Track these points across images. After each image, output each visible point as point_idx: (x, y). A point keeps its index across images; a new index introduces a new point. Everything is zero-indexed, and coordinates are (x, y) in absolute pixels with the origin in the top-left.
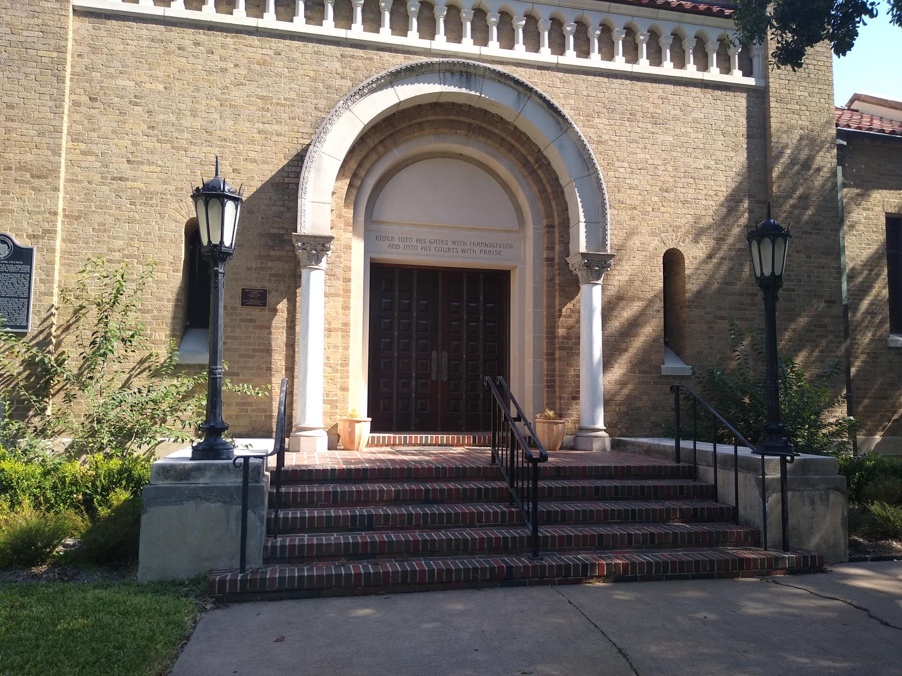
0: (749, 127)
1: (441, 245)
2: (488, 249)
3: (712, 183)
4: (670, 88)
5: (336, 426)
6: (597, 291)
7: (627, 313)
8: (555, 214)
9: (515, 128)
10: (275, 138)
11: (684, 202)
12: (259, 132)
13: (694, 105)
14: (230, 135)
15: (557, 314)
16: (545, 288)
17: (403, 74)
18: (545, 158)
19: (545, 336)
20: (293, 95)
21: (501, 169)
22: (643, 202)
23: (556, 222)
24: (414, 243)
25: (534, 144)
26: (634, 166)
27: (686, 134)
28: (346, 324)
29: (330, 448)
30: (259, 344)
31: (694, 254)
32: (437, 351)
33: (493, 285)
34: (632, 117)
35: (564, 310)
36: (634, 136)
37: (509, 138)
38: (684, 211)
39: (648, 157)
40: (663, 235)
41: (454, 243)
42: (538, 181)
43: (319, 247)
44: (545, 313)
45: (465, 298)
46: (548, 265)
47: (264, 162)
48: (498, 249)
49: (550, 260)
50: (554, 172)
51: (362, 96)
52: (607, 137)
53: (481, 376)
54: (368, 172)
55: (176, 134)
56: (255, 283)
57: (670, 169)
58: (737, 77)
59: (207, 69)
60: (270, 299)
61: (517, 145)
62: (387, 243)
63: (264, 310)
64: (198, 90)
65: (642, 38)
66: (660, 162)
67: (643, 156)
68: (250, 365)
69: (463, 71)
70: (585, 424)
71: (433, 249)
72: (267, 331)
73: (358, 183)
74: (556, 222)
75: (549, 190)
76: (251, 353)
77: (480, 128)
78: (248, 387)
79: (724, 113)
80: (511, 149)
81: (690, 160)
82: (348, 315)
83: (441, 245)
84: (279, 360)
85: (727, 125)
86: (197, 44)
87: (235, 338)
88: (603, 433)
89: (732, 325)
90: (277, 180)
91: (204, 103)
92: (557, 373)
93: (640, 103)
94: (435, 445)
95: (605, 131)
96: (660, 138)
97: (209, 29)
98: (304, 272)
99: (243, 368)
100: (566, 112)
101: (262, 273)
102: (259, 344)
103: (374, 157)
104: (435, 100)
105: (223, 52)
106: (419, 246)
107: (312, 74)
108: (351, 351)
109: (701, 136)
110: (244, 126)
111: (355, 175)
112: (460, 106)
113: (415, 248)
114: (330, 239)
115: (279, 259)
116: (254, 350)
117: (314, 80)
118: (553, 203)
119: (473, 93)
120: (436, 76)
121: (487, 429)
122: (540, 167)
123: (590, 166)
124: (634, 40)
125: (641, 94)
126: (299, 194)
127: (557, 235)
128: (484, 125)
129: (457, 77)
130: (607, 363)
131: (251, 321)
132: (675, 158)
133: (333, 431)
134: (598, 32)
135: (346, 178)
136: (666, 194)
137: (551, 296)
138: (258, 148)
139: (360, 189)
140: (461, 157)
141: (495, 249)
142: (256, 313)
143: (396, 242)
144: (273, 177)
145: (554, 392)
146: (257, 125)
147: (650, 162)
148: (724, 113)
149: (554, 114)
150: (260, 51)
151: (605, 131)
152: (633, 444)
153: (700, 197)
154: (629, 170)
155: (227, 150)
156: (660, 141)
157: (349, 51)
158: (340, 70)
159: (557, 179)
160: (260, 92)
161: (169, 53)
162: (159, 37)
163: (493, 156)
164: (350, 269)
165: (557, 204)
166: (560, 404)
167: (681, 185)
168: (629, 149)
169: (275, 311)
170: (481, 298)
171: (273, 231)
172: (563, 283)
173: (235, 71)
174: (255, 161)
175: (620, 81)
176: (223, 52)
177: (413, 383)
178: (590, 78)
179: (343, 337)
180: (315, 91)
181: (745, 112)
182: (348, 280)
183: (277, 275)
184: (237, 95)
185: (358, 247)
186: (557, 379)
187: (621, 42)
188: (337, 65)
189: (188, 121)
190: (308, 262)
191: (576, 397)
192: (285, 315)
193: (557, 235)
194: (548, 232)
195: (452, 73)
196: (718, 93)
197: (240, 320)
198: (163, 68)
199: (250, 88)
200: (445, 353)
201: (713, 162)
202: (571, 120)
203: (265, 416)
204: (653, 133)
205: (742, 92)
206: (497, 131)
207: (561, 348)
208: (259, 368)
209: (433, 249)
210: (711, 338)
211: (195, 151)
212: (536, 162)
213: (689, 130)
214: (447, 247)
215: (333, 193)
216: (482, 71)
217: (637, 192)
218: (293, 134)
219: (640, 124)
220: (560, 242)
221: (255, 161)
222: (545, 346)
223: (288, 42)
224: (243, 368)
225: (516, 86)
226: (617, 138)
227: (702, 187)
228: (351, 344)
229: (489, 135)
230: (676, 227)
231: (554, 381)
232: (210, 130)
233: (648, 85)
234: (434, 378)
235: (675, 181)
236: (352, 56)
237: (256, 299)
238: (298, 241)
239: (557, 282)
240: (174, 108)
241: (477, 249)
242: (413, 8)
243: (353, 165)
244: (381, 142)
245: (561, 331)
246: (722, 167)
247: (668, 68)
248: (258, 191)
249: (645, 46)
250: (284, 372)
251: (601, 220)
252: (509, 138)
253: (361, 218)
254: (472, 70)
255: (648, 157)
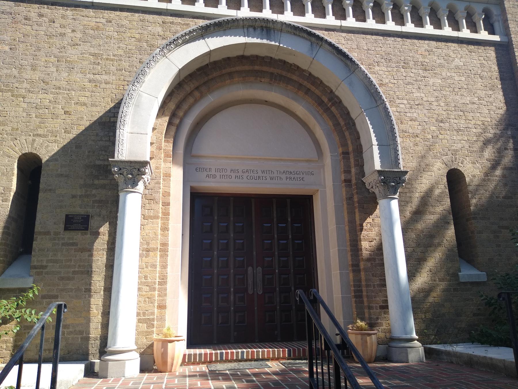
0: (500, 72)
1: (252, 174)
2: (292, 176)
3: (478, 115)
4: (433, 43)
5: (152, 345)
6: (395, 204)
7: (430, 218)
8: (349, 142)
9: (310, 74)
10: (103, 85)
11: (458, 130)
12: (90, 81)
13: (455, 56)
14: (64, 84)
15: (358, 228)
16: (345, 206)
17: (212, 28)
18: (337, 97)
19: (349, 249)
20: (121, 52)
21: (300, 109)
22: (424, 130)
23: (351, 149)
24: (228, 173)
25: (327, 86)
26: (412, 103)
27: (451, 77)
28: (165, 245)
29: (143, 370)
30: (79, 266)
31: (472, 171)
32: (253, 267)
33: (298, 209)
34: (406, 65)
35: (364, 224)
36: (409, 79)
37: (305, 83)
38: (459, 138)
39: (423, 95)
40: (444, 158)
41: (263, 172)
42: (333, 117)
43: (135, 172)
44: (347, 228)
45: (275, 220)
46: (346, 186)
47: (92, 105)
48: (301, 176)
49: (348, 181)
50: (346, 108)
51: (176, 46)
52: (387, 81)
53: (293, 289)
54: (186, 113)
55: (17, 85)
56: (78, 210)
57: (442, 104)
58: (483, 35)
59: (48, 34)
60: (93, 223)
61: (313, 88)
62: (205, 173)
63: (86, 234)
64: (39, 50)
65: (406, 8)
66: (433, 99)
67: (419, 94)
68: (70, 287)
69: (265, 28)
70: (397, 333)
71: (245, 177)
72: (87, 254)
73: (177, 121)
74: (351, 149)
75: (342, 123)
76: (71, 275)
77: (281, 76)
78: (30, 312)
79: (479, 62)
80: (308, 91)
81: (457, 97)
82: (167, 236)
83: (252, 174)
84: (98, 281)
85: (483, 71)
86: (41, 15)
87: (56, 261)
88: (417, 343)
89: (513, 234)
90: (104, 120)
91: (43, 60)
92: (363, 283)
93: (411, 54)
94: (251, 360)
95: (385, 76)
96: (431, 81)
97: (52, 5)
98: (121, 195)
99: (62, 290)
100: (354, 56)
101: (86, 199)
102: (79, 266)
103: (191, 100)
104: (240, 53)
105: (63, 22)
106: (234, 175)
107: (137, 36)
108: (169, 269)
109: (463, 79)
110: (77, 77)
111: (173, 116)
112: (263, 58)
113: (230, 177)
114: (145, 164)
115: (103, 187)
116: (74, 272)
117: (139, 40)
118: (347, 134)
119: (273, 43)
120: (241, 31)
121: (301, 338)
122: (333, 104)
123: (377, 98)
124: (400, 12)
125: (411, 48)
126: (118, 126)
127: (352, 161)
128: (284, 73)
129: (259, 31)
130: (411, 275)
131: (73, 244)
132: (445, 96)
133: (149, 351)
134: (372, 4)
135: (165, 116)
136: (442, 124)
137: (351, 213)
138: (88, 94)
139: (178, 127)
140: (266, 103)
141: (299, 176)
142: (78, 236)
143: (213, 172)
144: (101, 117)
145: (362, 302)
146: (88, 76)
147: (425, 99)
148: (479, 62)
149: (342, 58)
150: (94, 20)
151: (385, 76)
152: (448, 353)
153: (470, 126)
154: (408, 106)
155: (60, 96)
156: (431, 83)
157: (170, 19)
158: (161, 33)
159: (348, 113)
160: (92, 50)
161: (16, 23)
162: (8, 10)
163: (293, 99)
164: (169, 194)
165: (350, 134)
166: (370, 314)
167: (453, 117)
168: (406, 90)
169: (97, 234)
170: (289, 220)
171: (98, 163)
172: (361, 201)
173: (72, 35)
174: (85, 104)
175: (392, 39)
176: (63, 22)
177: (232, 298)
178: (369, 37)
179: (161, 256)
180: (140, 49)
181: (495, 61)
182: (166, 204)
183: (100, 201)
184: (73, 53)
185: (177, 174)
186: (364, 289)
187: (390, 12)
188: (159, 29)
189: (28, 74)
190: (125, 186)
191: (385, 307)
192: (106, 238)
193: (352, 161)
194: (344, 158)
195: (255, 29)
196: (472, 47)
197: (63, 244)
198: (9, 34)
199: (86, 47)
200: (260, 269)
201: (476, 99)
202: (358, 62)
203: (82, 338)
204: (425, 77)
205: (490, 46)
206: (295, 78)
207: (367, 271)
208: (78, 290)
209: (245, 177)
210: (499, 246)
211: (33, 98)
212: (330, 100)
213: (453, 74)
214: (258, 175)
215: (154, 129)
216: (279, 26)
217: (417, 123)
218: (120, 82)
219: (413, 71)
220: (356, 165)
221: (85, 104)
222: (350, 258)
223: (118, 13)
224: (62, 290)
225: (309, 37)
226: (395, 82)
227: (471, 118)
228: (169, 263)
229: (288, 81)
230: (454, 150)
231: (361, 291)
232: (47, 80)
233: (416, 41)
234: (250, 292)
235: (448, 114)
236: (172, 23)
237: (79, 224)
238: (115, 166)
239: (356, 199)
240: (17, 64)
241: (284, 176)
242: (321, 387)
243: (172, 106)
244: (197, 88)
245: (365, 245)
246: (484, 103)
247: (429, 29)
248: (86, 129)
249: (409, 14)
250: (102, 293)
251: (391, 142)
252: (305, 83)
253: (181, 151)
254: (271, 25)
255: (423, 95)
